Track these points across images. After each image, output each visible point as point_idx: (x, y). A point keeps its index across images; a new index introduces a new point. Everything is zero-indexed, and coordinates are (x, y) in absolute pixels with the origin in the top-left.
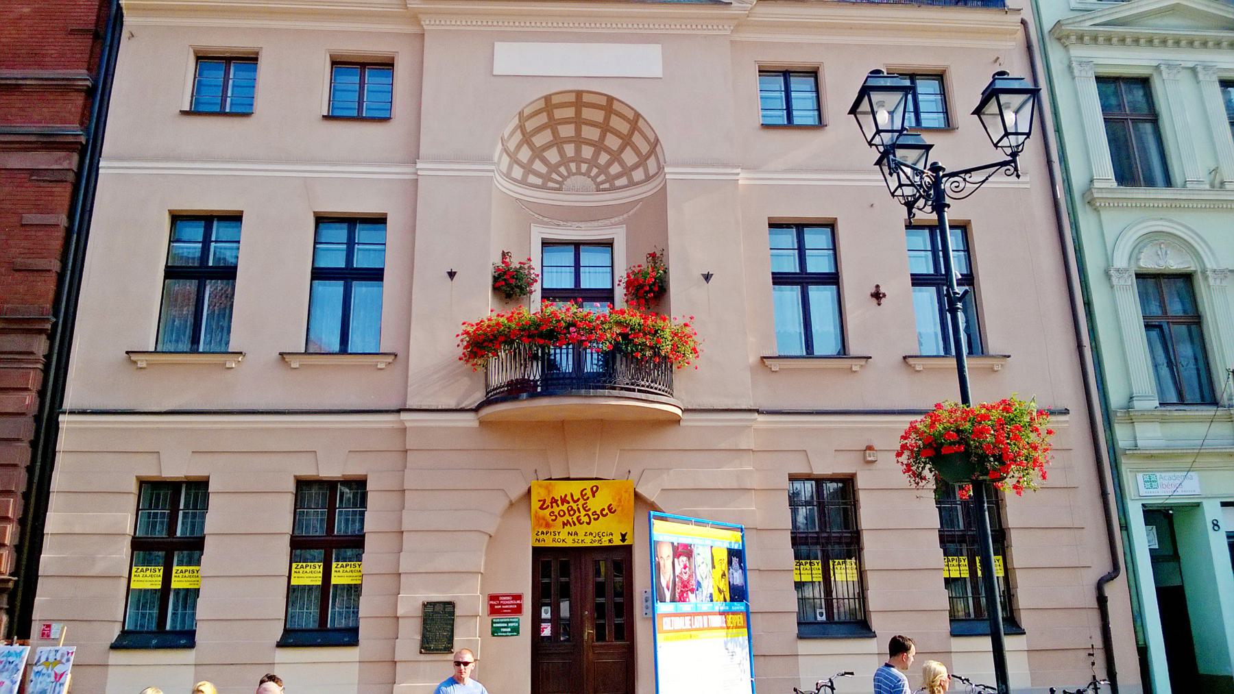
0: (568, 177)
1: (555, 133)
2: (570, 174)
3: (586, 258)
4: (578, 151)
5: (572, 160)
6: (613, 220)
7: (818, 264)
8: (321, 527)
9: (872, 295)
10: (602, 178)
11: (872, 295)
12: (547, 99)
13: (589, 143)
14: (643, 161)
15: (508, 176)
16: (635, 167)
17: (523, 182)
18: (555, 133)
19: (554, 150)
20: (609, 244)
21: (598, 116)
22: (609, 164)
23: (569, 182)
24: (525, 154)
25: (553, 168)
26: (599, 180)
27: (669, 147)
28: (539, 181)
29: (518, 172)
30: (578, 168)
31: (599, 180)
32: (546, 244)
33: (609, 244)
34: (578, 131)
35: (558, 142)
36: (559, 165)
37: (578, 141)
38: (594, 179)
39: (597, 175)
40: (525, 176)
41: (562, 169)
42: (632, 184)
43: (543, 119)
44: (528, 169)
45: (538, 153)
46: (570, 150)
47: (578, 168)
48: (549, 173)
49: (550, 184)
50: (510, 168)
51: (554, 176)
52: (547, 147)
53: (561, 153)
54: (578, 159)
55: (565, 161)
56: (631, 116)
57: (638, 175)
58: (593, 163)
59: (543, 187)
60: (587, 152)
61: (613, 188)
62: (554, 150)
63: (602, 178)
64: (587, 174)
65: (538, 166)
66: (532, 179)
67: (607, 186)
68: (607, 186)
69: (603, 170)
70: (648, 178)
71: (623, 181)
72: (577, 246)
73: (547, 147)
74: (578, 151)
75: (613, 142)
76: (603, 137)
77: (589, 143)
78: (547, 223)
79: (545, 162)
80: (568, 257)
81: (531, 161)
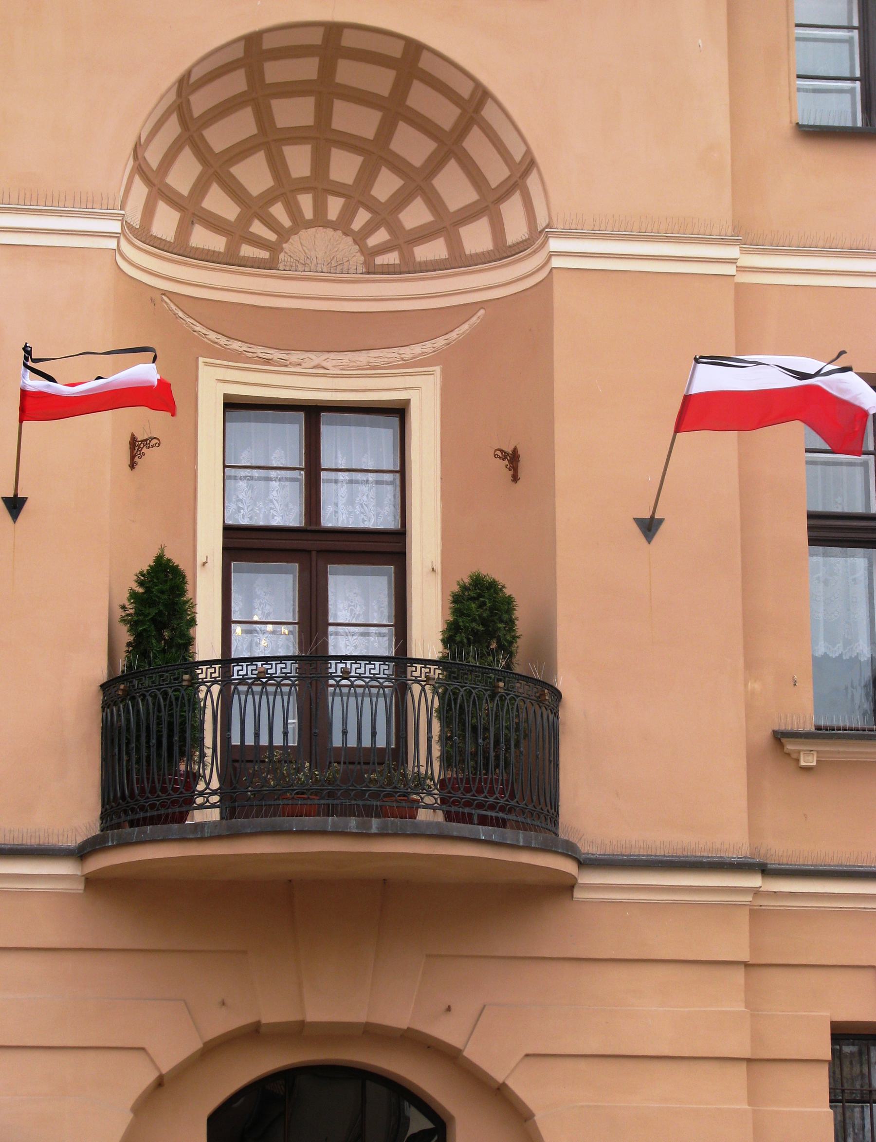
0: (295, 229)
1: (264, 118)
2: (299, 223)
3: (339, 444)
4: (320, 163)
5: (303, 185)
6: (408, 352)
7: (351, 506)
8: (294, 647)
9: (639, 522)
10: (381, 236)
11: (639, 522)
12: (252, 41)
13: (351, 143)
14: (488, 205)
15: (143, 235)
16: (469, 215)
17: (179, 249)
18: (264, 118)
19: (259, 159)
20: (397, 412)
21: (381, 81)
22: (401, 200)
23: (294, 246)
24: (183, 175)
25: (254, 207)
26: (373, 241)
27: (560, 186)
28: (217, 243)
29: (165, 223)
30: (320, 208)
31: (373, 241)
32: (233, 406)
33: (397, 412)
34: (323, 113)
35: (270, 141)
36: (269, 198)
37: (323, 138)
38: (359, 239)
39: (369, 229)
40: (184, 230)
41: (278, 211)
42: (459, 261)
43: (237, 83)
44: (191, 212)
45: (217, 170)
46: (299, 160)
47: (320, 208)
48: (244, 220)
49: (247, 251)
50: (149, 212)
51: (258, 228)
52: (241, 152)
53: (278, 166)
54: (320, 184)
55: (285, 189)
56: (465, 90)
57: (476, 237)
58: (357, 195)
59: (229, 259)
60: (344, 167)
61: (409, 268)
62: (259, 159)
63: (381, 236)
64: (343, 225)
65: (218, 202)
66: (203, 238)
67: (393, 258)
68: (393, 258)
69: (386, 214)
70: (503, 252)
71: (434, 250)
72: (313, 414)
73: (241, 152)
74: (320, 163)
75: (411, 145)
76: (386, 131)
77: (351, 143)
78: (237, 356)
79: (235, 191)
80: (284, 442)
81: (200, 188)
